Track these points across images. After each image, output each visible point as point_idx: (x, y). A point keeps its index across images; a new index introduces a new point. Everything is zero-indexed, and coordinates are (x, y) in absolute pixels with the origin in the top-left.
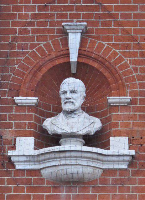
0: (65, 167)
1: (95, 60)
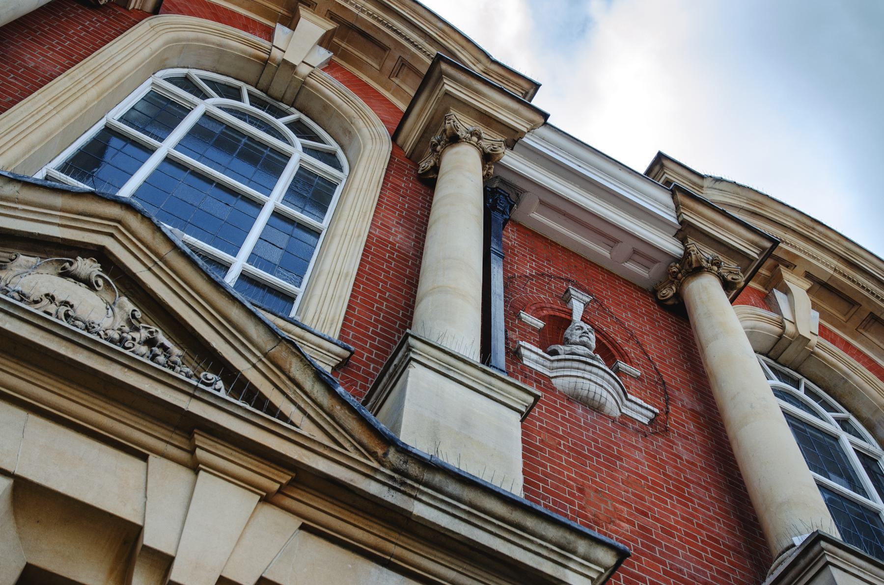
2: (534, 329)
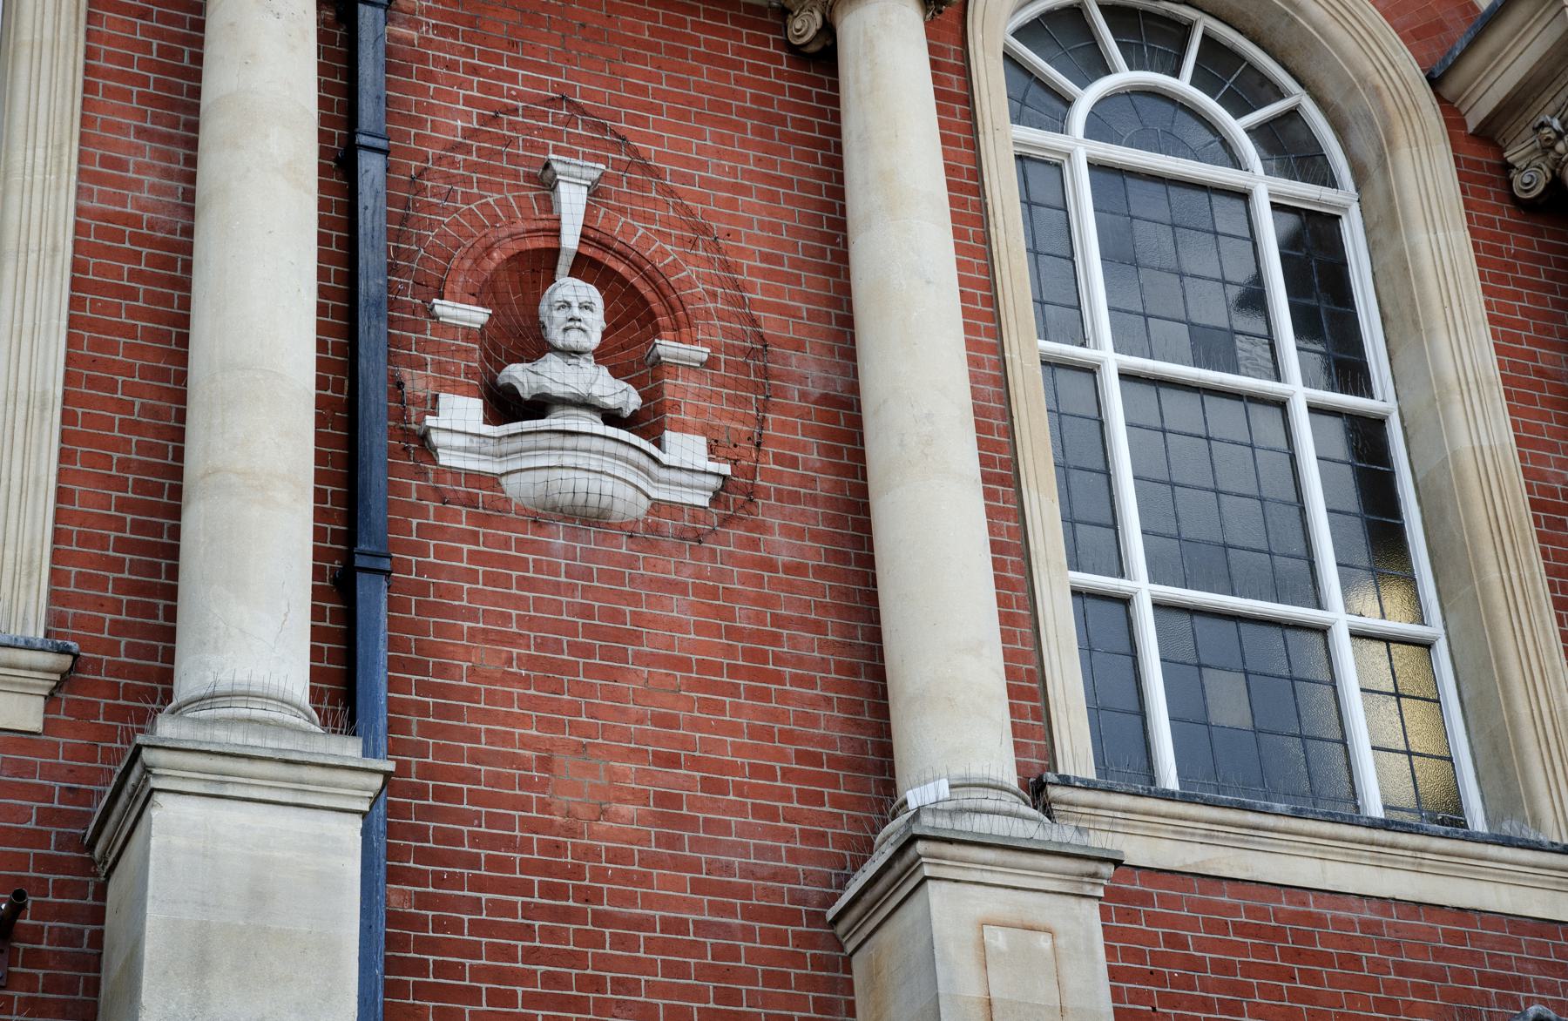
0: (572, 473)
1: (621, 255)
2: (468, 333)
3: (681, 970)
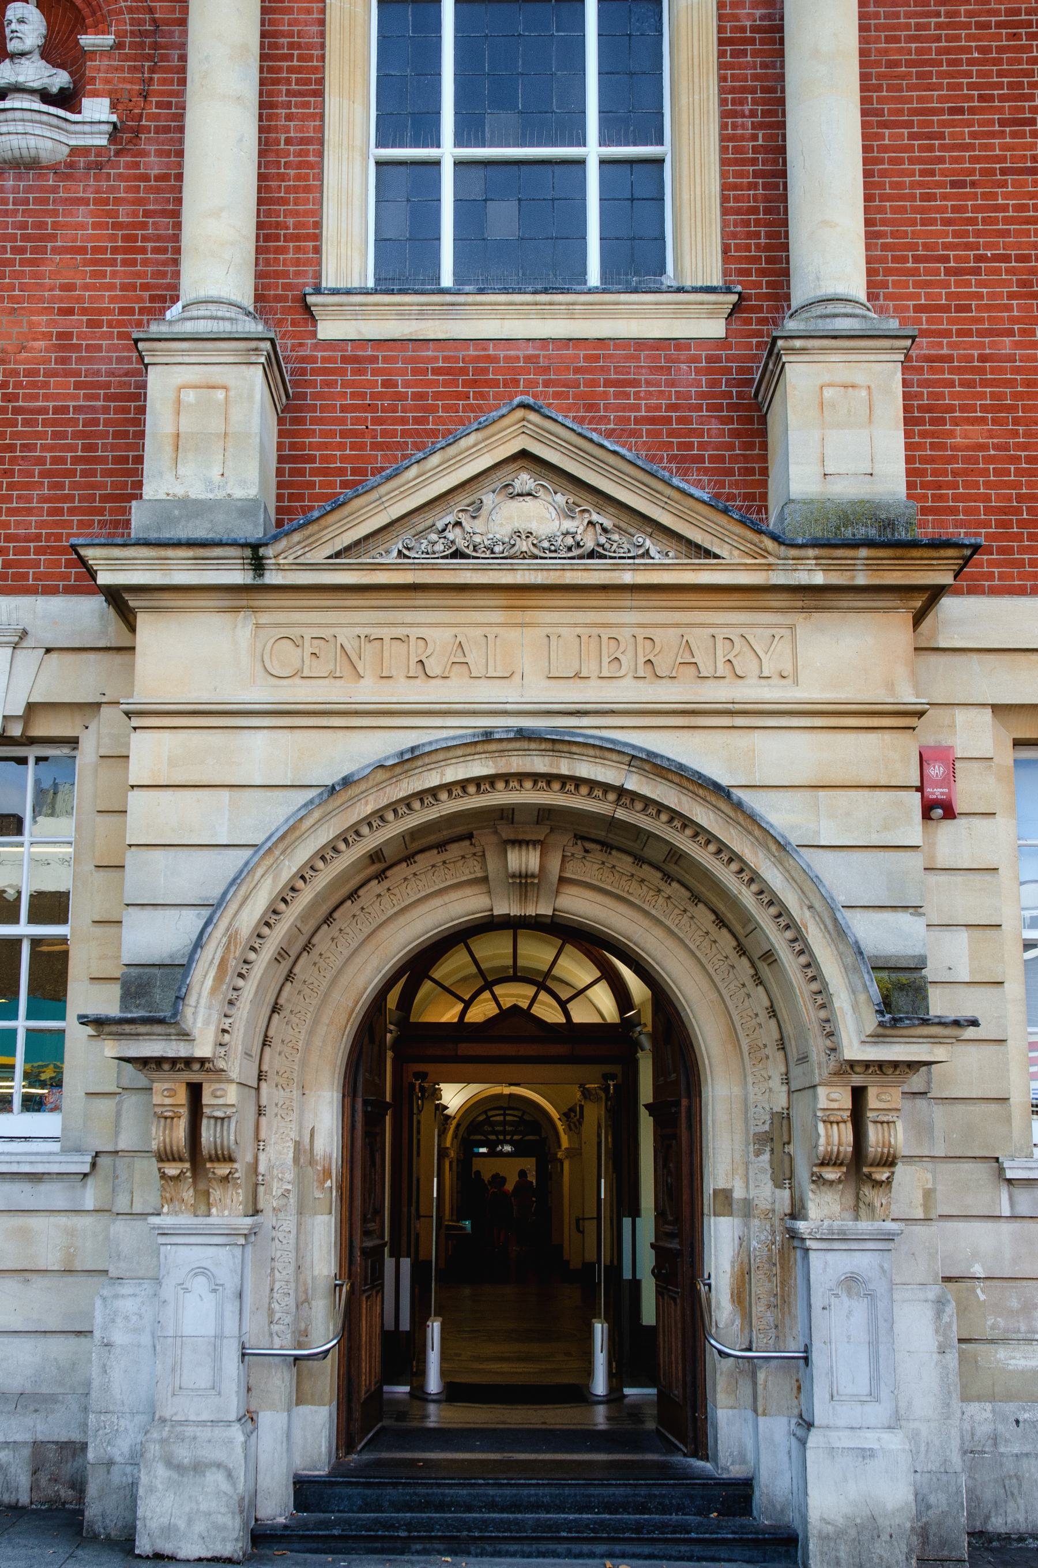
3: (63, 435)
